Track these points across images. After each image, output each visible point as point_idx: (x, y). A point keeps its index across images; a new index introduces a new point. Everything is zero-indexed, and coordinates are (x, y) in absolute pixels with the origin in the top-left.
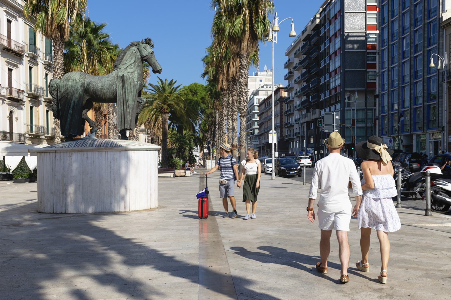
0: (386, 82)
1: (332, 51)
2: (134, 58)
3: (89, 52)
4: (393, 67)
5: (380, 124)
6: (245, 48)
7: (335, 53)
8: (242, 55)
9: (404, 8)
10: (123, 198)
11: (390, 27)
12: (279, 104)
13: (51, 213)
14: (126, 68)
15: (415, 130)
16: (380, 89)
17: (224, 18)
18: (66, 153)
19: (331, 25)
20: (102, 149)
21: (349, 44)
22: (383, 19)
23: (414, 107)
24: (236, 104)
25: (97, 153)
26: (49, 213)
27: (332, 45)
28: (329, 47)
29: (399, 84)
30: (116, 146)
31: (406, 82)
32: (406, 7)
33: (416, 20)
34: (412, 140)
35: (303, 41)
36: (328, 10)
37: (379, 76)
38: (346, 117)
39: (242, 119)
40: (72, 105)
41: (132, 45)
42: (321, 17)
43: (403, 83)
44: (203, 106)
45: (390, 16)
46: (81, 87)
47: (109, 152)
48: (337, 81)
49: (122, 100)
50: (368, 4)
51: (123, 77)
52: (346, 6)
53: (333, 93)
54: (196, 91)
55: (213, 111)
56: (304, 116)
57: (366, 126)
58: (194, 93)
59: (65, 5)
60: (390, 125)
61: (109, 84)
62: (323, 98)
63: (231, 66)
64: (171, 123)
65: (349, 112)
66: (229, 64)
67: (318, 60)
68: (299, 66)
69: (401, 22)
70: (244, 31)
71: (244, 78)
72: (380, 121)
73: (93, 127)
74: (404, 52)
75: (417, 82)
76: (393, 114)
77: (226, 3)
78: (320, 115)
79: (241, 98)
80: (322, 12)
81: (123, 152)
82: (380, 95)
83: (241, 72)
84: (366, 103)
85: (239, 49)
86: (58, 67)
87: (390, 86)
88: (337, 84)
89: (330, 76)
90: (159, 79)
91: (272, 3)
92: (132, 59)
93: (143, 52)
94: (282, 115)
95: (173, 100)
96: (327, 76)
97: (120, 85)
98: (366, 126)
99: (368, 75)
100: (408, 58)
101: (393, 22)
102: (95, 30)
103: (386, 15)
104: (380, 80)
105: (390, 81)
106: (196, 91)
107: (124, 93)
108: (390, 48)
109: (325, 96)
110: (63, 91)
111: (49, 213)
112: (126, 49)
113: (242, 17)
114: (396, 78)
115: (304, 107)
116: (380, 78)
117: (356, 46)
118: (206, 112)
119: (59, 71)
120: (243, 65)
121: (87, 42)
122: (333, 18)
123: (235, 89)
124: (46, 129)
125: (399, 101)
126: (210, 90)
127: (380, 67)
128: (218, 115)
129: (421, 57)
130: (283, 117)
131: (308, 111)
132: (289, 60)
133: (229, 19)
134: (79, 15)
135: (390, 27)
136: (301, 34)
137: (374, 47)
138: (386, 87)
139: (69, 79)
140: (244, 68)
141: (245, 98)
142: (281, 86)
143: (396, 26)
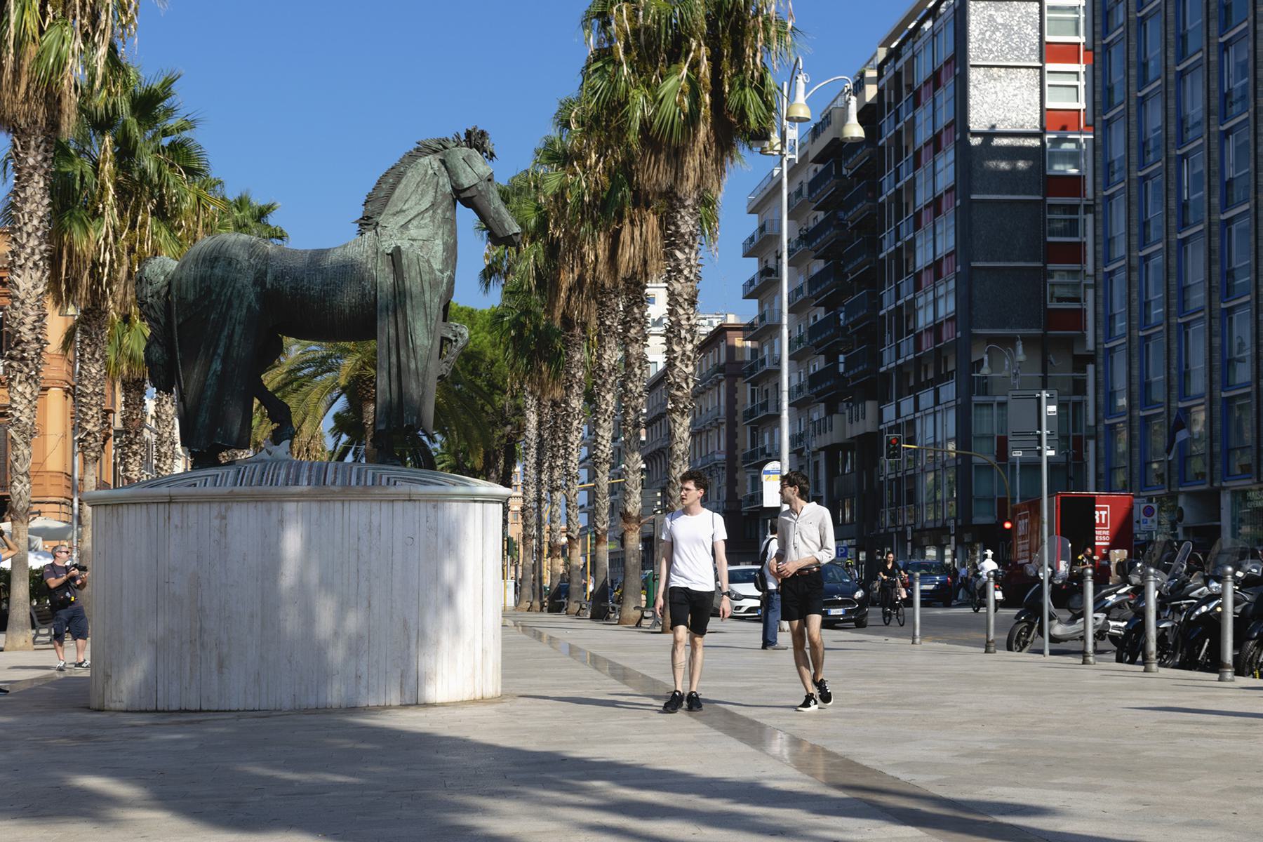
0: (1119, 308)
1: (923, 197)
2: (431, 193)
3: (121, 178)
4: (1147, 258)
5: (1102, 453)
6: (692, 174)
7: (936, 205)
8: (681, 200)
9: (1182, 55)
11: (1133, 119)
12: (723, 384)
13: (146, 711)
14: (405, 226)
15: (1227, 475)
16: (1100, 332)
17: (626, 69)
18: (206, 507)
19: (921, 109)
22: (1109, 90)
23: (1224, 395)
24: (638, 372)
26: (141, 711)
27: (922, 176)
28: (912, 185)
29: (1168, 315)
31: (1192, 307)
32: (1190, 52)
33: (1226, 97)
34: (1219, 508)
35: (816, 161)
36: (910, 54)
37: (1095, 286)
39: (679, 419)
41: (423, 150)
42: (884, 81)
43: (1182, 311)
45: (1133, 81)
46: (255, 284)
47: (354, 505)
48: (941, 303)
50: (1048, 38)
52: (973, 45)
53: (927, 344)
60: (1137, 458)
62: (889, 362)
63: (625, 235)
64: (351, 443)
65: (985, 411)
66: (618, 233)
67: (871, 228)
69: (1172, 104)
70: (692, 119)
71: (687, 278)
72: (1101, 444)
74: (1184, 207)
75: (1230, 311)
76: (1146, 419)
77: (630, 20)
78: (881, 421)
79: (676, 348)
80: (885, 62)
82: (1101, 352)
83: (676, 259)
86: (29, 228)
87: (1135, 323)
88: (941, 313)
89: (918, 287)
91: (790, 25)
92: (423, 195)
93: (461, 173)
94: (736, 424)
96: (906, 284)
99: (1053, 285)
100: (1201, 227)
101: (1142, 101)
103: (1117, 77)
104: (1100, 301)
105: (1135, 304)
108: (1134, 191)
109: (898, 357)
111: (141, 711)
112: (401, 161)
113: (685, 71)
114: (1156, 295)
115: (818, 395)
116: (1101, 293)
119: (33, 242)
120: (683, 236)
121: (116, 143)
122: (926, 83)
123: (635, 320)
125: (1169, 373)
126: (517, 325)
127: (1100, 256)
128: (533, 419)
129: (1245, 222)
130: (738, 430)
131: (831, 410)
132: (762, 228)
135: (1133, 119)
136: (807, 139)
137: (1073, 185)
138: (1120, 325)
142: (732, 319)
143: (1155, 117)
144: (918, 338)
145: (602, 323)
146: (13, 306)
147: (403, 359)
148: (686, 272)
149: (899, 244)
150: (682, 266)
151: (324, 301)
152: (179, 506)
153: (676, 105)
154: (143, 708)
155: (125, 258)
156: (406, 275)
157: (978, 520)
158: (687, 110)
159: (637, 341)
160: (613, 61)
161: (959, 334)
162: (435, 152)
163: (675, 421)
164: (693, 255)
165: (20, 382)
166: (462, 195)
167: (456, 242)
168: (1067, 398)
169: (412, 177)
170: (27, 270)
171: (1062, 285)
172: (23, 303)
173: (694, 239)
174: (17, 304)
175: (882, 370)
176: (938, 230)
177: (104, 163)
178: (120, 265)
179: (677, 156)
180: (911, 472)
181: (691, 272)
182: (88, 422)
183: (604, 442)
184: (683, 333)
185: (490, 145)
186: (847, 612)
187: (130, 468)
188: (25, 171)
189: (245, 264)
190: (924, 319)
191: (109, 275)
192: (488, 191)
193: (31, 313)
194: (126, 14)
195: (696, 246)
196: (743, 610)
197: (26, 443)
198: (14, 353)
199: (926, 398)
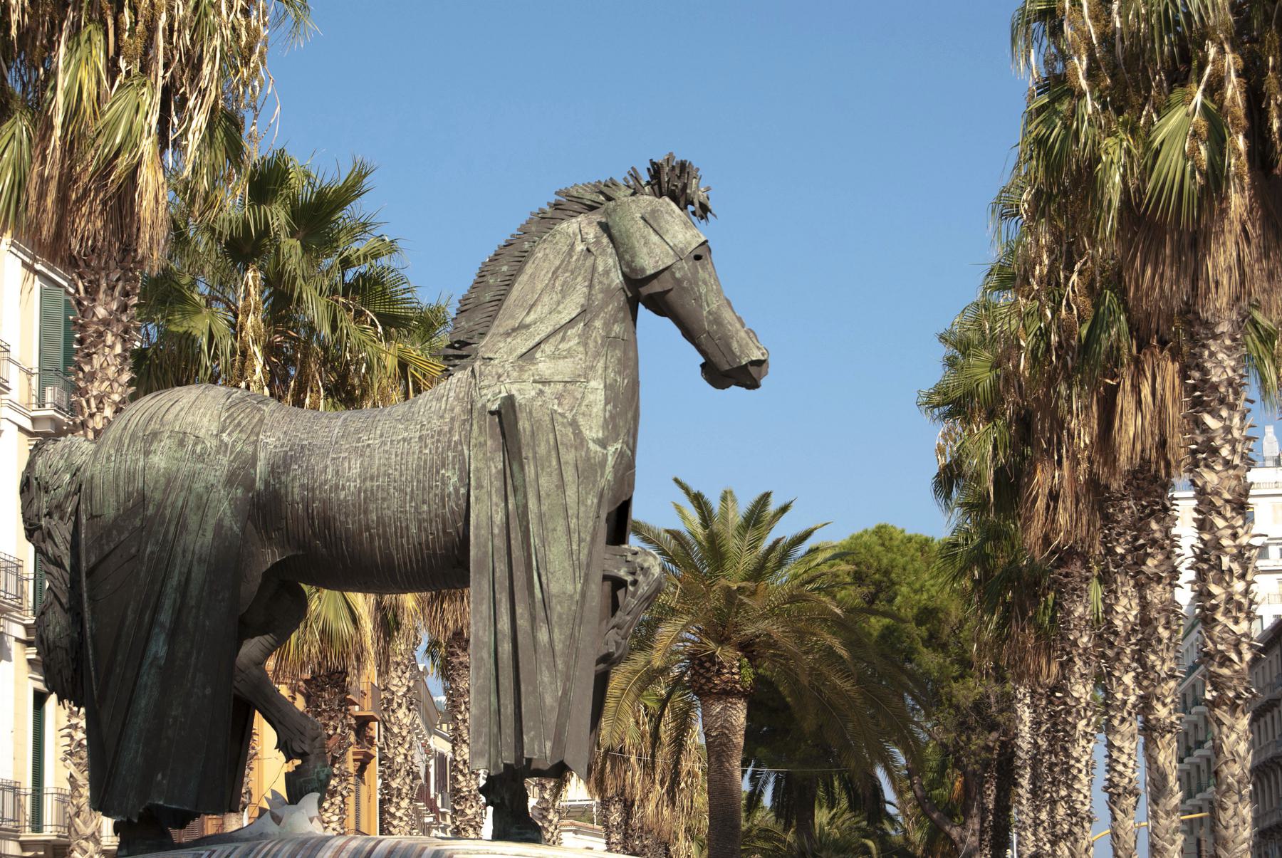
2: (582, 289)
8: (1207, 324)
14: (528, 356)
24: (1165, 634)
39: (1227, 719)
44: (930, 660)
46: (230, 481)
49: (501, 568)
51: (505, 417)
54: (887, 573)
55: (995, 689)
58: (878, 584)
59: (145, 69)
61: (413, 461)
63: (1125, 401)
66: (1113, 391)
71: (1227, 464)
73: (303, 756)
77: (1095, 18)
79: (1215, 589)
83: (1206, 430)
85: (1185, 285)
90: (687, 490)
92: (564, 294)
93: (639, 245)
95: (772, 613)
97: (486, 464)
102: (319, 218)
106: (887, 573)
112: (524, 231)
113: (1198, 97)
118: (950, 697)
120: (1215, 387)
121: (267, 281)
123: (1154, 542)
124: (28, 802)
126: (978, 557)
133: (1119, 112)
134: (226, 127)
140: (1222, 401)
141: (1239, 586)
145: (1111, 552)
147: (523, 623)
148: (1225, 452)
150: (1218, 442)
151: (365, 512)
153: (1186, 157)
159: (1159, 580)
162: (592, 208)
163: (1220, 723)
164: (1236, 420)
166: (645, 291)
167: (635, 385)
169: (545, 258)
173: (1237, 393)
179: (1196, 243)
181: (1234, 451)
183: (1124, 758)
184: (1226, 561)
185: (698, 190)
188: (91, 330)
189: (211, 443)
194: (247, 64)
195: (1241, 404)
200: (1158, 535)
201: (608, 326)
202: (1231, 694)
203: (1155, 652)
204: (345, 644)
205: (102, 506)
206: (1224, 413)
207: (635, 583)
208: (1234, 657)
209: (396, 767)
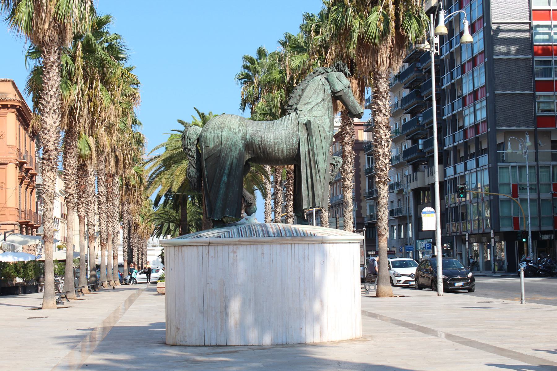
2: (322, 94)
8: (379, 75)
10: (317, 319)
13: (199, 346)
14: (311, 110)
17: (350, 11)
18: (227, 247)
20: (288, 240)
21: (500, 45)
24: (350, 160)
25: (278, 246)
26: (197, 346)
30: (305, 235)
38: (500, 181)
40: (227, 168)
46: (242, 140)
47: (296, 246)
48: (478, 113)
49: (308, 161)
51: (308, 125)
53: (471, 135)
56: (410, 179)
57: (539, 198)
61: (285, 135)
65: (505, 170)
68: (396, 82)
71: (384, 114)
78: (445, 176)
79: (379, 150)
81: (317, 246)
83: (378, 105)
84: (536, 154)
86: (52, 93)
88: (479, 118)
89: (464, 104)
92: (318, 95)
94: (360, 176)
96: (458, 103)
97: (303, 137)
98: (539, 198)
99: (539, 103)
107: (311, 151)
109: (454, 141)
110: (212, 145)
111: (197, 346)
113: (381, 10)
115: (408, 162)
117: (513, 49)
119: (54, 100)
120: (381, 93)
123: (347, 133)
130: (361, 179)
139: (224, 127)
140: (383, 97)
144: (465, 132)
146: (43, 132)
148: (384, 111)
149: (453, 81)
150: (382, 109)
152: (213, 247)
154: (198, 344)
155: (86, 104)
156: (313, 134)
157: (504, 229)
158: (382, 29)
159: (349, 144)
160: (344, 5)
161: (489, 130)
162: (322, 74)
163: (380, 188)
165: (48, 171)
168: (548, 163)
170: (51, 114)
171: (544, 103)
172: (49, 131)
174: (46, 132)
175: (445, 148)
176: (475, 74)
177: (79, 56)
178: (84, 107)
179: (375, 52)
180: (464, 203)
181: (386, 111)
182: (69, 189)
184: (383, 142)
186: (464, 284)
187: (80, 210)
188: (49, 64)
189: (237, 130)
190: (469, 121)
191: (79, 114)
192: (348, 92)
193: (53, 136)
196: (401, 282)
197: (52, 202)
198: (45, 156)
199: (471, 163)
200: (349, 131)
201: (328, 103)
202: (384, 180)
203: (347, 165)
204: (86, 156)
205: (209, 144)
206: (384, 100)
207: (337, 165)
208: (385, 169)
209: (90, 194)
